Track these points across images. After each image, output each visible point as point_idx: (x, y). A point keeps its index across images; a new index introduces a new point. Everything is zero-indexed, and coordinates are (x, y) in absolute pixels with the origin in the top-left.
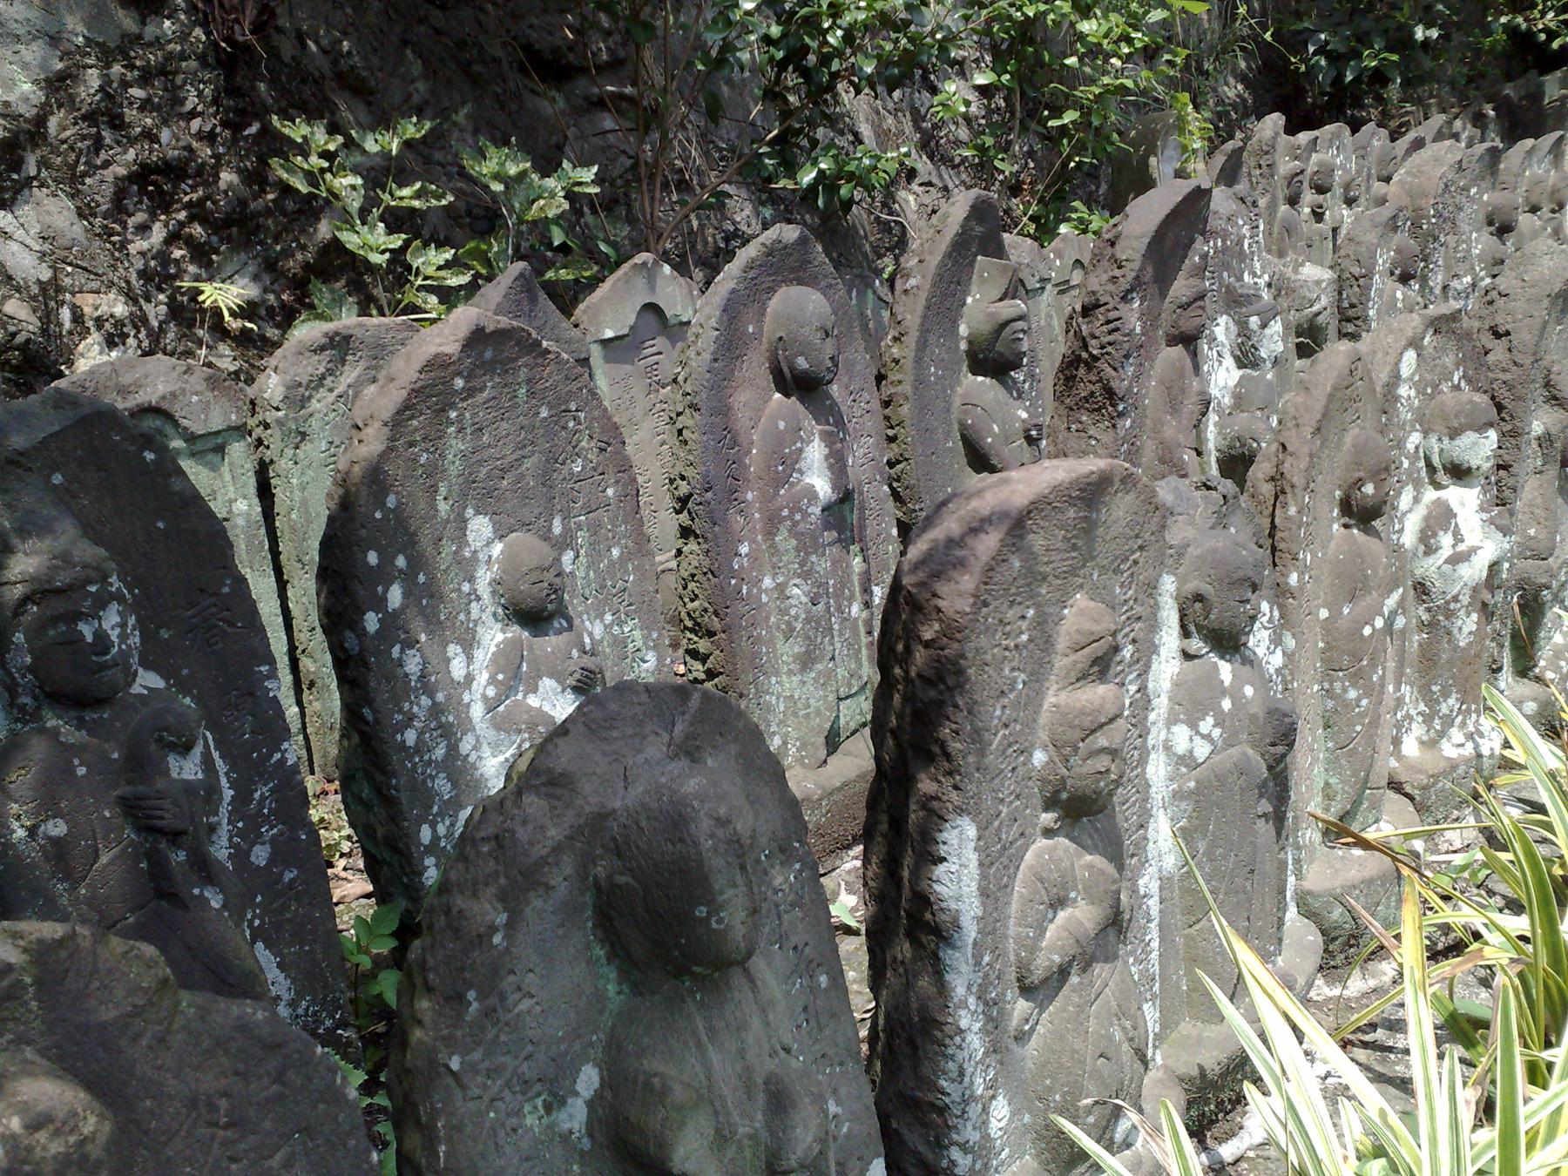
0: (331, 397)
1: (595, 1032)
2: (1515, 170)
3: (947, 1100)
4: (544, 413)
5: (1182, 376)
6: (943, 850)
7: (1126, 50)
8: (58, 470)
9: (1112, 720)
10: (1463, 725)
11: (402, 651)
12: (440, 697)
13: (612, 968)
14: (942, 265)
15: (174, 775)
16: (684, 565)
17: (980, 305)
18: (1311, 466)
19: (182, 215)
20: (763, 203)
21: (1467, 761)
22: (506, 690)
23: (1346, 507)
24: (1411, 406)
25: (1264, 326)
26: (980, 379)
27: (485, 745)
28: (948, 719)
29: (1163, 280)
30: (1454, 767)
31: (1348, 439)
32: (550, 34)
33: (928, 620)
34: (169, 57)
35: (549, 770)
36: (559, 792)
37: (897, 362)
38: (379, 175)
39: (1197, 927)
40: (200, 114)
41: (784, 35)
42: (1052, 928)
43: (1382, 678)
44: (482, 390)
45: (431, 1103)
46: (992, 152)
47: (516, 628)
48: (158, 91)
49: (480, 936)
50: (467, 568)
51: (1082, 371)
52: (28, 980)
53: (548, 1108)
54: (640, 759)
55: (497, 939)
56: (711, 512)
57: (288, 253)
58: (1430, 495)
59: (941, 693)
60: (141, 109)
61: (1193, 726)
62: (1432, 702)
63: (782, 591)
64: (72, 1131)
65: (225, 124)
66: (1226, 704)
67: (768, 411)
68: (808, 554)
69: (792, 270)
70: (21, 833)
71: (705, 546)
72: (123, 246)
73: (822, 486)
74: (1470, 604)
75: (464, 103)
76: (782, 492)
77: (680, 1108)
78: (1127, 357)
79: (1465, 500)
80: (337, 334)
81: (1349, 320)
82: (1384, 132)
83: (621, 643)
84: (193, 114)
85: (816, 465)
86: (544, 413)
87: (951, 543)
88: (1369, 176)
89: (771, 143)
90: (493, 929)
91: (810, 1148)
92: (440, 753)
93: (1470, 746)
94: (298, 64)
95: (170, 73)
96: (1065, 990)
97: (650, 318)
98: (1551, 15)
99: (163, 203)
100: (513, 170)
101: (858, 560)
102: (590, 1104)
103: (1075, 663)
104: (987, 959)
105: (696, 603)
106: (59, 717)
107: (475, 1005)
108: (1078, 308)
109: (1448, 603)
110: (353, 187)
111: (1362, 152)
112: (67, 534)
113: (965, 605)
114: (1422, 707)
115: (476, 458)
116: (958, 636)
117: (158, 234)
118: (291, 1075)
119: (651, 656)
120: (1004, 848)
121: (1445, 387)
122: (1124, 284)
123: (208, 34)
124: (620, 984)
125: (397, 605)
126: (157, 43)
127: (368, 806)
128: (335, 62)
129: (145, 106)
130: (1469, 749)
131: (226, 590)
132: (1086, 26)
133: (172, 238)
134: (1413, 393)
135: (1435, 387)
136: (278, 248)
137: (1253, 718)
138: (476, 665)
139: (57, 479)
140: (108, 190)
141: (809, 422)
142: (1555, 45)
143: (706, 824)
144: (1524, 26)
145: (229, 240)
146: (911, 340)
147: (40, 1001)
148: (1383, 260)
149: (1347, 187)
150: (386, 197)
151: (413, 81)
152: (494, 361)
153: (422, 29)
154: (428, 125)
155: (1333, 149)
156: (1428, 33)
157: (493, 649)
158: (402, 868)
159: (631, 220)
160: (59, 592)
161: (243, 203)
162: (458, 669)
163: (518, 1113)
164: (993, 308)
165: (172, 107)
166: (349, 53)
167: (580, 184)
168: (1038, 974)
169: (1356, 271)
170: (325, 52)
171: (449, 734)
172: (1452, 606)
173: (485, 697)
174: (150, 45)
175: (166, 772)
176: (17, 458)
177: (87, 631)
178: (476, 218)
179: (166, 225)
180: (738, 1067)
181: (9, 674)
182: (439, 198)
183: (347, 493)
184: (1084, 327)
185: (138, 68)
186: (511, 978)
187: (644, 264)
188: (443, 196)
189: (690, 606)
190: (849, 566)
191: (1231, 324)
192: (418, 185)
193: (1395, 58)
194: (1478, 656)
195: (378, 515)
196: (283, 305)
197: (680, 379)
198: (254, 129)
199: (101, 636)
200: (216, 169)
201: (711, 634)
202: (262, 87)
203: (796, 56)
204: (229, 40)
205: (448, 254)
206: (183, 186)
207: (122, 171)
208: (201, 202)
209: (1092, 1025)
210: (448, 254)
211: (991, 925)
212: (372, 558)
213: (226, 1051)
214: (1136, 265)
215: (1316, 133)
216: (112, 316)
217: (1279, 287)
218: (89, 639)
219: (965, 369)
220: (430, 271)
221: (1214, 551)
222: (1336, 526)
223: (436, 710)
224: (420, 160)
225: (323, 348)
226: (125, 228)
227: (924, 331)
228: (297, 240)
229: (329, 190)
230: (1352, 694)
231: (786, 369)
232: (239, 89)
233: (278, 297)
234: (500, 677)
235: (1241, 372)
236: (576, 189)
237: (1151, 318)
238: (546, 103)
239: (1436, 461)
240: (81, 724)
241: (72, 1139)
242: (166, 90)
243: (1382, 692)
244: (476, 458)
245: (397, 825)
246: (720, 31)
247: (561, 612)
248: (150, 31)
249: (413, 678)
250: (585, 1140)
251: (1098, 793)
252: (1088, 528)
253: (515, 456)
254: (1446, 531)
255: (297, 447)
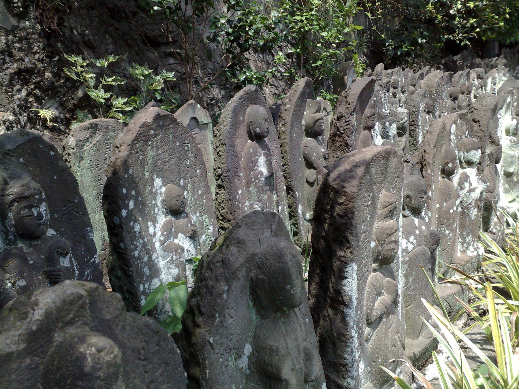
0: (91, 145)
1: (249, 332)
2: (457, 81)
3: (347, 361)
4: (178, 144)
5: (368, 140)
6: (346, 274)
7: (337, 41)
8: (22, 157)
9: (396, 231)
10: (473, 245)
11: (134, 223)
12: (146, 240)
13: (254, 309)
14: (297, 101)
15: (62, 264)
16: (219, 197)
17: (309, 115)
18: (434, 157)
19: (32, 86)
20: (222, 89)
21: (475, 257)
22: (167, 238)
23: (443, 171)
24: (454, 142)
25: (390, 125)
26: (309, 138)
27: (160, 257)
28: (349, 229)
29: (362, 109)
30: (472, 259)
31: (443, 150)
32: (153, 31)
33: (341, 196)
34: (28, 34)
35: (238, 238)
36: (241, 246)
37: (284, 132)
38: (101, 74)
39: (409, 307)
40: (38, 53)
41: (233, 32)
42: (377, 302)
43: (456, 226)
44: (159, 135)
45: (204, 355)
46: (294, 74)
47: (170, 216)
48: (25, 45)
49: (220, 294)
50: (154, 195)
51: (337, 138)
52: (88, 301)
53: (236, 360)
54: (264, 236)
55: (225, 296)
56: (230, 179)
57: (68, 101)
58: (461, 171)
59: (346, 220)
60: (19, 50)
61: (407, 239)
62: (464, 238)
63: (252, 206)
64: (112, 353)
65: (47, 57)
66: (417, 232)
67: (246, 146)
68: (261, 194)
69: (253, 100)
70: (9, 285)
71: (227, 191)
72: (12, 96)
73: (265, 171)
74: (475, 206)
75: (125, 53)
76: (252, 173)
77: (283, 356)
78: (352, 133)
79: (472, 172)
80: (93, 123)
81: (412, 125)
82: (412, 71)
83: (202, 223)
84: (36, 53)
85: (262, 164)
86: (178, 144)
87: (347, 171)
88: (408, 84)
89: (228, 68)
90: (224, 292)
91: (318, 373)
92: (146, 259)
93: (476, 252)
94: (71, 37)
95: (28, 39)
96: (381, 324)
97: (194, 122)
98: (461, 35)
99: (26, 82)
100: (147, 73)
101: (275, 196)
102: (249, 358)
103: (384, 212)
104: (359, 312)
105: (224, 211)
106: (23, 243)
107: (218, 319)
108: (336, 117)
109: (468, 205)
110: (91, 78)
111: (406, 77)
112: (27, 179)
113: (355, 190)
114: (460, 240)
115: (157, 158)
116: (352, 200)
117: (24, 93)
118: (161, 343)
119: (211, 228)
120: (363, 275)
121: (463, 137)
122: (351, 110)
123: (41, 26)
124: (256, 315)
125: (132, 208)
126: (24, 29)
127: (119, 279)
128: (83, 38)
129: (20, 50)
130: (475, 253)
131: (76, 201)
132: (323, 34)
133: (29, 94)
134: (455, 138)
135: (461, 136)
136: (64, 99)
137: (425, 237)
138: (157, 229)
139: (21, 160)
140: (8, 77)
141: (260, 150)
142: (462, 44)
143: (289, 257)
144: (452, 39)
145: (48, 95)
146: (288, 125)
147: (90, 309)
148: (422, 106)
149: (402, 88)
150: (103, 81)
151: (109, 45)
152: (162, 125)
153: (111, 28)
154: (117, 57)
155: (399, 75)
156: (422, 41)
157: (162, 224)
158: (133, 300)
159: (180, 93)
160: (26, 198)
161: (53, 83)
162: (151, 230)
163: (227, 360)
164: (313, 115)
165: (29, 50)
166: (88, 34)
167: (169, 78)
168: (373, 318)
169: (414, 110)
170: (79, 34)
171: (149, 252)
172: (469, 206)
173: (160, 240)
174: (21, 29)
175: (59, 264)
176: (8, 152)
177: (35, 211)
178: (130, 91)
179: (27, 90)
180: (295, 344)
181: (6, 227)
182: (121, 81)
183: (115, 169)
184: (338, 124)
185: (18, 37)
186: (227, 310)
187: (192, 104)
188: (122, 81)
189: (221, 212)
190: (273, 198)
191: (380, 125)
192: (114, 77)
193: (413, 48)
194: (477, 223)
195: (126, 176)
196: (66, 118)
197: (218, 135)
198: (57, 58)
199: (39, 214)
200: (44, 71)
201: (229, 221)
202: (59, 45)
203: (237, 39)
204: (49, 28)
205: (125, 100)
206: (33, 77)
207: (12, 71)
208: (39, 82)
209: (390, 335)
210: (125, 100)
211: (360, 299)
212: (124, 191)
213: (142, 333)
214: (355, 104)
215: (393, 70)
216: (9, 120)
217: (392, 113)
218: (36, 215)
219: (304, 135)
220: (120, 105)
221: (412, 181)
222: (440, 178)
223: (144, 245)
224: (112, 69)
225: (88, 128)
226: (13, 90)
227: (292, 122)
228: (71, 96)
229: (84, 79)
230: (447, 232)
231: (252, 132)
232: (52, 45)
233: (65, 115)
234: (165, 233)
235: (383, 140)
236: (168, 79)
237: (359, 121)
238: (151, 54)
239: (462, 160)
240: (31, 246)
241: (112, 356)
242: (27, 45)
243: (456, 231)
244: (157, 158)
245: (132, 285)
246: (214, 29)
247: (183, 211)
248: (22, 25)
249: (137, 233)
250: (247, 371)
251: (391, 256)
252: (386, 167)
253: (169, 158)
254: (467, 182)
255: (80, 162)
